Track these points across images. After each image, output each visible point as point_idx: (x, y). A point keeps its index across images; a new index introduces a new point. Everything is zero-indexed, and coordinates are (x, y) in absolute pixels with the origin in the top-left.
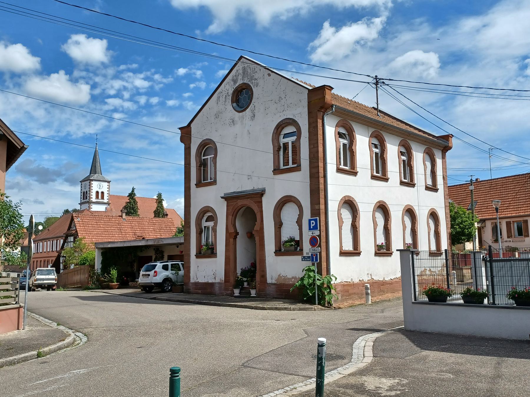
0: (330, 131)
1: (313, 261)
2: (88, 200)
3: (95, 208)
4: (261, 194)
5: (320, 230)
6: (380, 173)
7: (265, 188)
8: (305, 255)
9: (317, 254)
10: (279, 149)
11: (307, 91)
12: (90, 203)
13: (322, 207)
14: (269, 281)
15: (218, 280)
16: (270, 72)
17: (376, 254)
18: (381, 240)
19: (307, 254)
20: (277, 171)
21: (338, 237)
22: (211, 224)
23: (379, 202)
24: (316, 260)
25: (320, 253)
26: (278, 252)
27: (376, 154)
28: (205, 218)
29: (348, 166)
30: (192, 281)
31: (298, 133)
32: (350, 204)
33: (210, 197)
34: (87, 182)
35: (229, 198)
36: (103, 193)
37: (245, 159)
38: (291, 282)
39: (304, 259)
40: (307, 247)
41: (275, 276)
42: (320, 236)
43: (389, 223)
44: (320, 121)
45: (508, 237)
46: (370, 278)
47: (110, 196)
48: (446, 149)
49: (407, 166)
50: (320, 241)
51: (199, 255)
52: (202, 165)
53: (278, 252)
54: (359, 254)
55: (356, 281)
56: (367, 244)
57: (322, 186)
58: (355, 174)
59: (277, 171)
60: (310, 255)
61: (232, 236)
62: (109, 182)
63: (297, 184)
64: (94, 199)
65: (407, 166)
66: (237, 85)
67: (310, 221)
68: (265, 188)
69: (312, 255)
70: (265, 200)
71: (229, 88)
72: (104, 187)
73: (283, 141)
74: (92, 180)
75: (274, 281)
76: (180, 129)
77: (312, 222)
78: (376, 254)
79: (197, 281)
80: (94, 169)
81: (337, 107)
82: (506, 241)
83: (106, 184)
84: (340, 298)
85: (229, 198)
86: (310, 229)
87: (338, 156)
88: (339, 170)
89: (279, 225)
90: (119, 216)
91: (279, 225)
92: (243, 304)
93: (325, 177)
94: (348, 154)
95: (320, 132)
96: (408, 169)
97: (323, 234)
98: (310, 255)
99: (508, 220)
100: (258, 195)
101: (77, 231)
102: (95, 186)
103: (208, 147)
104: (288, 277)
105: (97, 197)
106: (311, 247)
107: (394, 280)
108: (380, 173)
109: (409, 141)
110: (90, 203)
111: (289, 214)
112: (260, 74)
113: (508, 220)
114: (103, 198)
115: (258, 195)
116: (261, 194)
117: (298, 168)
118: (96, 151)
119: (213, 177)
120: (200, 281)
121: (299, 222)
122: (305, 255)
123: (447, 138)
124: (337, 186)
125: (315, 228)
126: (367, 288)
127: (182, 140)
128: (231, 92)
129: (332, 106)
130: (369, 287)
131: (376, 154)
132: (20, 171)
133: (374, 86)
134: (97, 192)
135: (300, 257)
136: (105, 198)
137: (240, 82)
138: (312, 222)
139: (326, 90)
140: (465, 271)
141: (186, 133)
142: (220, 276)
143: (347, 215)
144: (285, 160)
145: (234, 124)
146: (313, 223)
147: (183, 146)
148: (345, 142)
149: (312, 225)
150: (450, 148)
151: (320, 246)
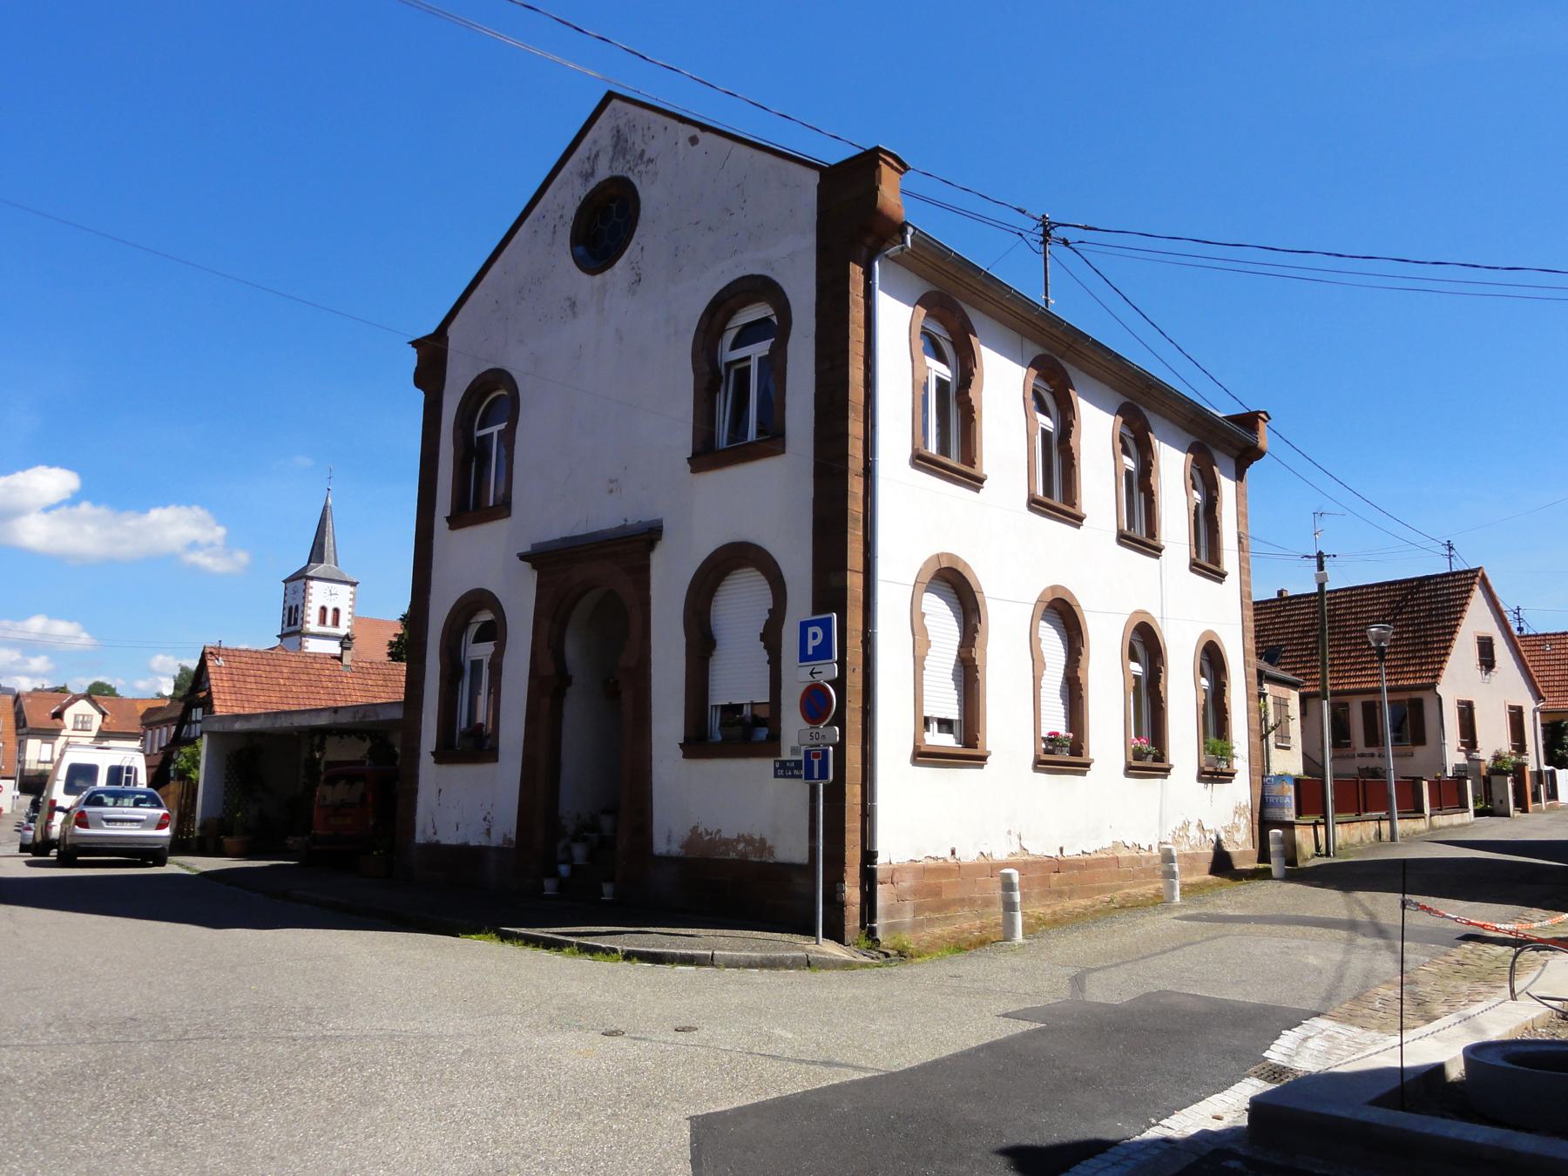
0: (895, 319)
1: (809, 776)
2: (297, 627)
3: (313, 646)
4: (650, 535)
5: (842, 663)
6: (1057, 495)
7: (661, 521)
8: (786, 755)
9: (826, 752)
10: (711, 378)
11: (813, 178)
12: (301, 634)
13: (855, 581)
14: (660, 846)
15: (496, 840)
16: (696, 131)
17: (1040, 765)
18: (1055, 721)
19: (794, 751)
20: (706, 456)
21: (907, 677)
22: (484, 651)
23: (1054, 588)
24: (824, 775)
25: (840, 748)
26: (697, 744)
27: (1046, 435)
28: (473, 630)
29: (953, 453)
30: (420, 838)
31: (777, 330)
32: (954, 584)
33: (486, 559)
34: (300, 583)
35: (542, 558)
36: (336, 611)
37: (609, 433)
38: (733, 855)
39: (785, 770)
40: (794, 730)
41: (681, 832)
42: (840, 684)
43: (1082, 663)
44: (856, 271)
45: (1368, 743)
46: (1016, 849)
47: (357, 620)
48: (1245, 455)
49: (1140, 488)
50: (841, 704)
51: (447, 753)
52: (472, 455)
53: (697, 744)
54: (980, 760)
55: (968, 855)
56: (1012, 722)
57: (855, 507)
58: (975, 482)
59: (706, 456)
60: (801, 757)
61: (548, 686)
62: (354, 584)
63: (764, 501)
64: (313, 625)
65: (1140, 488)
66: (593, 184)
67: (804, 626)
68: (661, 521)
69: (807, 753)
70: (659, 561)
71: (568, 197)
72: (341, 597)
73: (728, 355)
74: (312, 578)
75: (676, 849)
76: (415, 344)
77: (811, 630)
78: (1040, 765)
79: (435, 838)
80: (317, 553)
81: (923, 240)
82: (1362, 755)
83: (349, 588)
84: (908, 918)
85: (542, 558)
86: (804, 657)
87: (919, 410)
88: (920, 460)
89: (701, 643)
90: (334, 657)
91: (701, 643)
92: (536, 932)
93: (869, 472)
94: (955, 409)
95: (857, 314)
96: (1139, 499)
97: (854, 680)
98: (801, 757)
99: (1369, 698)
100: (635, 545)
101: (210, 693)
102: (319, 594)
103: (495, 396)
104: (725, 835)
105: (323, 621)
106: (808, 726)
107: (1094, 856)
108: (1057, 495)
109: (1147, 413)
110: (301, 634)
111: (740, 606)
112: (664, 141)
113: (1369, 698)
114: (336, 623)
115: (635, 545)
116: (650, 535)
117: (773, 440)
118: (325, 508)
119: (502, 491)
120: (444, 841)
121: (771, 637)
122: (786, 755)
123: (1249, 421)
124: (911, 518)
125: (823, 652)
126: (1008, 886)
127: (420, 379)
128: (570, 213)
129: (902, 228)
130: (1016, 878)
131: (1046, 435)
132: (1479, 1030)
133: (1037, 246)
134: (324, 609)
135: (766, 765)
136: (341, 622)
137: (603, 173)
138: (811, 630)
139: (885, 169)
140: (1298, 831)
141: (432, 358)
142: (506, 823)
143: (942, 619)
144: (730, 426)
145: (574, 314)
146: (815, 636)
147: (420, 395)
148: (945, 372)
149: (812, 643)
150: (1260, 454)
151: (840, 720)
